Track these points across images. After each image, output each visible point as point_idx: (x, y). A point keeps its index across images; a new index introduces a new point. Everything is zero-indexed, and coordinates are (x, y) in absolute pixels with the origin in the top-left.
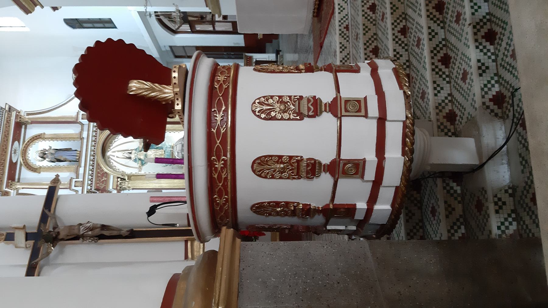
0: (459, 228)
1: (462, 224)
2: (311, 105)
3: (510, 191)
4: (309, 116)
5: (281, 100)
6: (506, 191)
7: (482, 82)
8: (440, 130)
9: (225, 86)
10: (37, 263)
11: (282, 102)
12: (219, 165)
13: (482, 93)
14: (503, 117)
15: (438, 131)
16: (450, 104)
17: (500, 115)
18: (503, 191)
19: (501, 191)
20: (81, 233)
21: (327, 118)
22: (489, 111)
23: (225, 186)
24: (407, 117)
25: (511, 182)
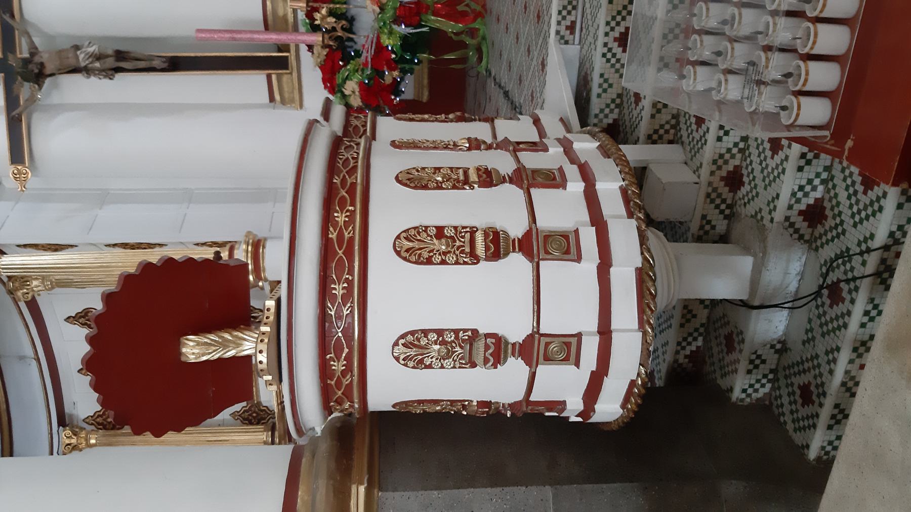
0: (695, 339)
1: (700, 334)
2: (491, 355)
3: (778, 346)
4: (487, 259)
5: (441, 339)
6: (772, 347)
7: (798, 182)
8: (708, 200)
9: (346, 382)
10: (20, 115)
11: (443, 343)
12: (338, 366)
13: (790, 200)
14: (812, 244)
15: (705, 202)
16: (739, 156)
17: (807, 237)
18: (769, 346)
19: (765, 345)
20: (83, 64)
21: (517, 262)
22: (791, 230)
23: (348, 332)
24: (639, 375)
25: (785, 334)
